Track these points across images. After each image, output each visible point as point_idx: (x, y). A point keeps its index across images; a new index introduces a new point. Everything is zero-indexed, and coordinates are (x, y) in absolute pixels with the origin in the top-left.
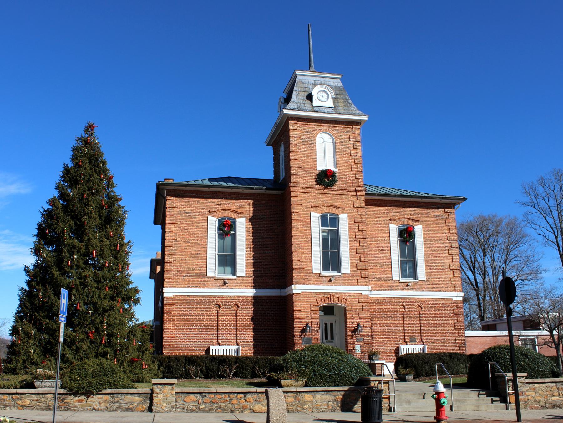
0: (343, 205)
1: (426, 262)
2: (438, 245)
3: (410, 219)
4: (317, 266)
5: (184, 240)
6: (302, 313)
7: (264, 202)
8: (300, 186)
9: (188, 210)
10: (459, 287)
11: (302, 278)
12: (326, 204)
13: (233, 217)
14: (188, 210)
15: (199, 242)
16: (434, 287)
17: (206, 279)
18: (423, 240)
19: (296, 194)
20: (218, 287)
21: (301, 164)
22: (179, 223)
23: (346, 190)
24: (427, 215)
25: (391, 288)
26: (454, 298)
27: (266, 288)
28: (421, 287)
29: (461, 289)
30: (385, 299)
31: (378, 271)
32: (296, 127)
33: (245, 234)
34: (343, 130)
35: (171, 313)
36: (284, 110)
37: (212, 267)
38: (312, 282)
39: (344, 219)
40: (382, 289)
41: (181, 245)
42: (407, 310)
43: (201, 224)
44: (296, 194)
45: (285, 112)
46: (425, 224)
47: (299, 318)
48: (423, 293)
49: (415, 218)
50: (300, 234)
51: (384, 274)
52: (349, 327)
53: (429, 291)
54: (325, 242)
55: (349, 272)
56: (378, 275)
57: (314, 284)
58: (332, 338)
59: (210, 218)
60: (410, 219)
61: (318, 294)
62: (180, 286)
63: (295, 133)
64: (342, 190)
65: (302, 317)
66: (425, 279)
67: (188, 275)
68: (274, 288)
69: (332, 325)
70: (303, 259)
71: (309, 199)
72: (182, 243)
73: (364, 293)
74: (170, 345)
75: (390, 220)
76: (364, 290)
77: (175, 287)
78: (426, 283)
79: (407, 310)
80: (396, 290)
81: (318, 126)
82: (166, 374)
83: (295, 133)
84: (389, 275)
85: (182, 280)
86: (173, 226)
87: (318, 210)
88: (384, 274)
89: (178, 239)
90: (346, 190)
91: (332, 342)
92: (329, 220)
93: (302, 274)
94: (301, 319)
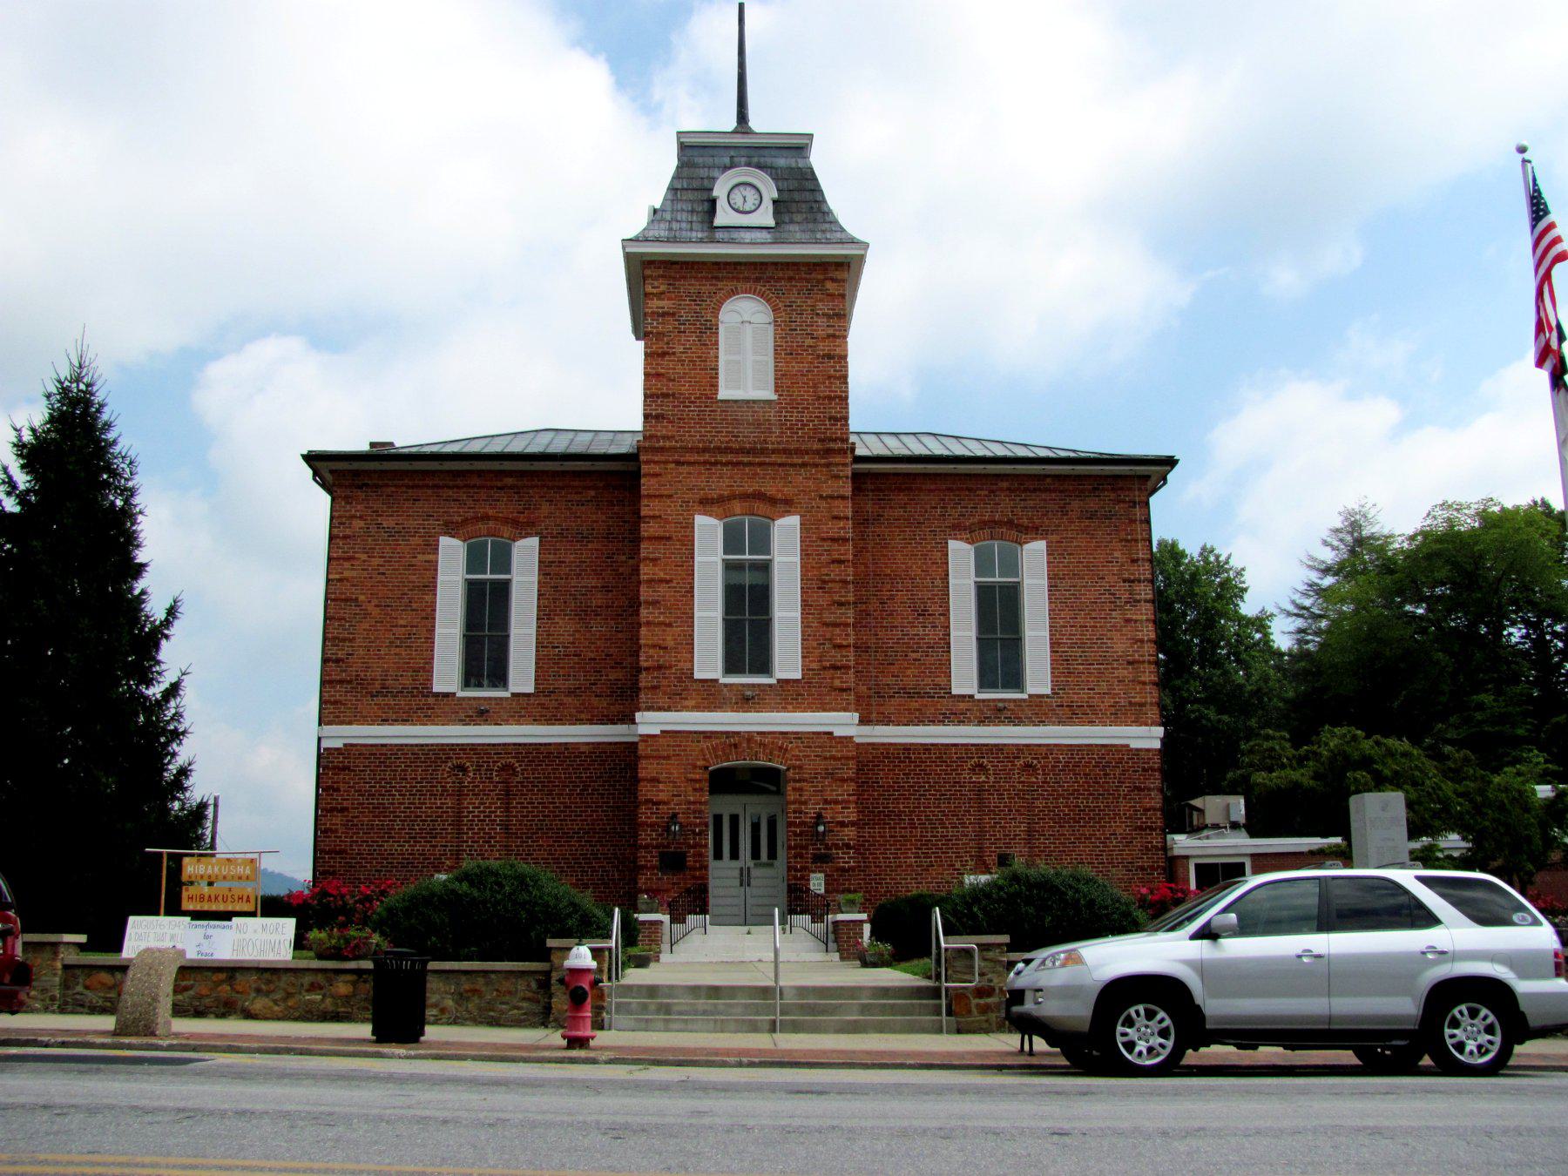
1: (1055, 644)
4: (708, 661)
5: (375, 602)
7: (592, 493)
10: (1153, 713)
11: (665, 693)
12: (738, 490)
15: (414, 606)
17: (431, 700)
18: (1046, 582)
22: (364, 557)
23: (798, 452)
26: (1134, 744)
27: (591, 722)
28: (1037, 710)
29: (1156, 717)
31: (909, 672)
32: (663, 288)
33: (536, 579)
35: (338, 790)
38: (691, 703)
40: (920, 722)
41: (367, 615)
42: (992, 779)
43: (420, 557)
46: (1055, 538)
47: (651, 801)
48: (1041, 730)
50: (662, 575)
54: (733, 595)
55: (799, 676)
56: (910, 682)
57: (697, 708)
58: (772, 854)
61: (708, 735)
64: (785, 451)
65: (662, 796)
66: (1048, 691)
67: (384, 691)
68: (613, 723)
69: (772, 824)
70: (670, 643)
72: (370, 608)
73: (838, 732)
74: (334, 873)
76: (843, 723)
78: (1054, 702)
79: (992, 779)
80: (961, 722)
83: (661, 303)
84: (941, 680)
86: (347, 565)
89: (362, 598)
90: (798, 452)
91: (771, 865)
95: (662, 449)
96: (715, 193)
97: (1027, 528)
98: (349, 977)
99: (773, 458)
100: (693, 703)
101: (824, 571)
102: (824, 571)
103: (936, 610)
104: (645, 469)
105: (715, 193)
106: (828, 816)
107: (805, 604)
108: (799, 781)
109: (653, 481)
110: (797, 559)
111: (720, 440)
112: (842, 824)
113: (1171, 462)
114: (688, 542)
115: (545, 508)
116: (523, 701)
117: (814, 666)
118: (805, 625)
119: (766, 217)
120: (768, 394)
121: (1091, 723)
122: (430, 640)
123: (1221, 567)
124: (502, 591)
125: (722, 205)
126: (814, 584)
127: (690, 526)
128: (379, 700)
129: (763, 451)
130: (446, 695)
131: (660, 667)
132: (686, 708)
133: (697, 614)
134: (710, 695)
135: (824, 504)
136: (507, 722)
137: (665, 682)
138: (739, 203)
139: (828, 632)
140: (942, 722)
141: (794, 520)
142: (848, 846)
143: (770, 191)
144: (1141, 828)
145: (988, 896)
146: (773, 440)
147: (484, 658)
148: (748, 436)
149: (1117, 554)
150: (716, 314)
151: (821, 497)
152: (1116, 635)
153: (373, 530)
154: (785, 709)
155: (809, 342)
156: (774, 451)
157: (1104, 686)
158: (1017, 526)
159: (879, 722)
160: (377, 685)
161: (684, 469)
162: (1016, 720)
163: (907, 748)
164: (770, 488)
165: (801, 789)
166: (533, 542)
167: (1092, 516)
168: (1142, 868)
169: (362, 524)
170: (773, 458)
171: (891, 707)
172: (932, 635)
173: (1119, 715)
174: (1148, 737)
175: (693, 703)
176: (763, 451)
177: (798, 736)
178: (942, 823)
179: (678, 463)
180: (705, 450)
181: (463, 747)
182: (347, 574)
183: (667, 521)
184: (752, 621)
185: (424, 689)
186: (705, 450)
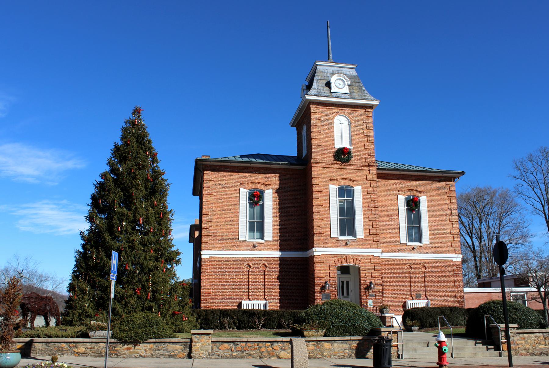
0: (357, 178)
2: (440, 213)
3: (415, 190)
4: (335, 232)
5: (219, 209)
7: (289, 176)
10: (458, 250)
16: (437, 250)
17: (238, 242)
18: (427, 209)
20: (249, 250)
21: (320, 143)
22: (214, 194)
23: (360, 165)
25: (399, 251)
26: (454, 260)
27: (290, 250)
29: (460, 252)
30: (394, 260)
31: (388, 236)
32: (316, 111)
38: (330, 245)
39: (358, 190)
40: (392, 252)
46: (429, 195)
47: (319, 277)
50: (320, 204)
53: (433, 253)
54: (342, 211)
55: (363, 237)
56: (388, 239)
57: (332, 247)
59: (242, 190)
60: (415, 190)
61: (336, 256)
64: (356, 165)
65: (322, 276)
67: (222, 239)
68: (297, 251)
69: (348, 282)
70: (323, 225)
71: (328, 174)
72: (217, 211)
73: (376, 255)
75: (399, 191)
76: (376, 252)
81: (336, 110)
82: (203, 325)
83: (316, 116)
86: (209, 196)
89: (214, 208)
90: (360, 165)
91: (348, 297)
94: (321, 277)
95: (319, 163)
98: (313, 343)
100: (331, 245)
109: (316, 173)
110: (361, 200)
113: (463, 174)
116: (268, 243)
121: (441, 253)
123: (166, 190)
131: (320, 233)
134: (336, 243)
137: (322, 238)
138: (338, 85)
140: (398, 252)
153: (217, 185)
154: (359, 248)
157: (445, 241)
160: (220, 237)
161: (326, 169)
169: (214, 183)
174: (457, 258)
175: (331, 245)
177: (363, 256)
181: (249, 258)
182: (209, 200)
183: (321, 186)
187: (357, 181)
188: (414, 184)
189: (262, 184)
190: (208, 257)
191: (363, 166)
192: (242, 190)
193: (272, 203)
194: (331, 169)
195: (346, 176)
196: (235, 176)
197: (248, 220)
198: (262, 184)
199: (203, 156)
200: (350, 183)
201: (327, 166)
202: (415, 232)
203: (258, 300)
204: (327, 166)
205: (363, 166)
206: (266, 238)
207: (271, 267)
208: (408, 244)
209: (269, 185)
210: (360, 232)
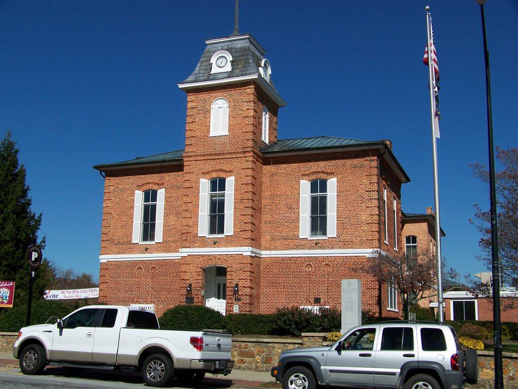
0: (231, 168)
2: (353, 198)
3: (323, 172)
6: (187, 274)
8: (192, 154)
9: (121, 187)
13: (155, 189)
14: (121, 187)
15: (128, 214)
16: (345, 244)
17: (132, 246)
18: (336, 194)
19: (189, 163)
20: (141, 253)
21: (194, 134)
22: (113, 199)
23: (234, 153)
24: (344, 165)
25: (297, 247)
28: (331, 244)
30: (290, 258)
31: (284, 230)
34: (235, 93)
36: (179, 85)
37: (305, 229)
39: (230, 181)
40: (288, 249)
44: (189, 163)
45: (180, 87)
49: (329, 171)
50: (189, 200)
51: (291, 233)
52: (229, 287)
53: (340, 248)
56: (285, 234)
57: (199, 247)
59: (137, 192)
60: (323, 172)
62: (113, 253)
63: (192, 104)
65: (187, 278)
70: (191, 224)
71: (200, 167)
72: (115, 215)
75: (303, 175)
77: (109, 254)
81: (214, 94)
82: (162, 327)
83: (192, 104)
85: (114, 248)
86: (109, 202)
87: (207, 176)
88: (291, 233)
90: (234, 153)
92: (218, 185)
93: (189, 238)
94: (186, 280)
95: (191, 156)
96: (211, 62)
97: (330, 173)
99: (227, 156)
101: (242, 196)
102: (242, 196)
103: (294, 207)
104: (185, 164)
105: (211, 62)
106: (240, 284)
107: (235, 208)
108: (231, 272)
111: (211, 151)
112: (245, 287)
114: (198, 188)
115: (167, 178)
116: (159, 245)
117: (238, 230)
118: (235, 216)
119: (228, 68)
120: (227, 133)
121: (352, 248)
122: (132, 225)
124: (154, 208)
125: (214, 66)
126: (238, 201)
127: (198, 183)
128: (117, 246)
129: (223, 154)
130: (136, 244)
132: (196, 247)
133: (200, 214)
134: (203, 242)
135: (243, 171)
136: (154, 252)
139: (243, 218)
141: (163, 190)
142: (247, 295)
143: (230, 58)
144: (369, 289)
145: (57, 302)
146: (228, 149)
147: (217, 224)
148: (218, 149)
149: (364, 181)
150: (210, 105)
151: (242, 169)
152: (363, 213)
155: (241, 112)
156: (226, 154)
158: (326, 173)
159: (274, 249)
162: (323, 248)
163: (283, 258)
164: (225, 168)
165: (231, 275)
166: (163, 190)
167: (355, 167)
168: (369, 304)
170: (227, 156)
171: (278, 243)
172: (293, 216)
173: (362, 245)
175: (198, 245)
176: (223, 154)
178: (294, 286)
179: (195, 160)
180: (204, 155)
184: (218, 215)
185: (130, 242)
186: (204, 155)
187: (231, 172)
188: (322, 165)
189: (155, 184)
190: (105, 261)
191: (238, 153)
192: (137, 192)
193: (163, 203)
194: (203, 161)
195: (218, 167)
196: (132, 179)
197: (142, 222)
198: (155, 184)
199: (137, 158)
200: (222, 175)
201: (199, 158)
202: (319, 223)
203: (147, 303)
204: (199, 158)
205: (238, 153)
206: (226, 233)
207: (160, 270)
208: (309, 239)
209: (163, 184)
210: (229, 228)
